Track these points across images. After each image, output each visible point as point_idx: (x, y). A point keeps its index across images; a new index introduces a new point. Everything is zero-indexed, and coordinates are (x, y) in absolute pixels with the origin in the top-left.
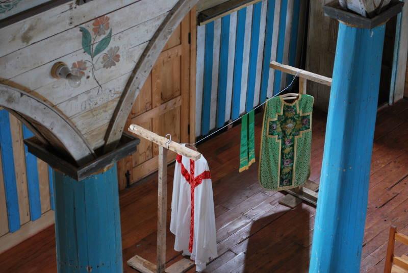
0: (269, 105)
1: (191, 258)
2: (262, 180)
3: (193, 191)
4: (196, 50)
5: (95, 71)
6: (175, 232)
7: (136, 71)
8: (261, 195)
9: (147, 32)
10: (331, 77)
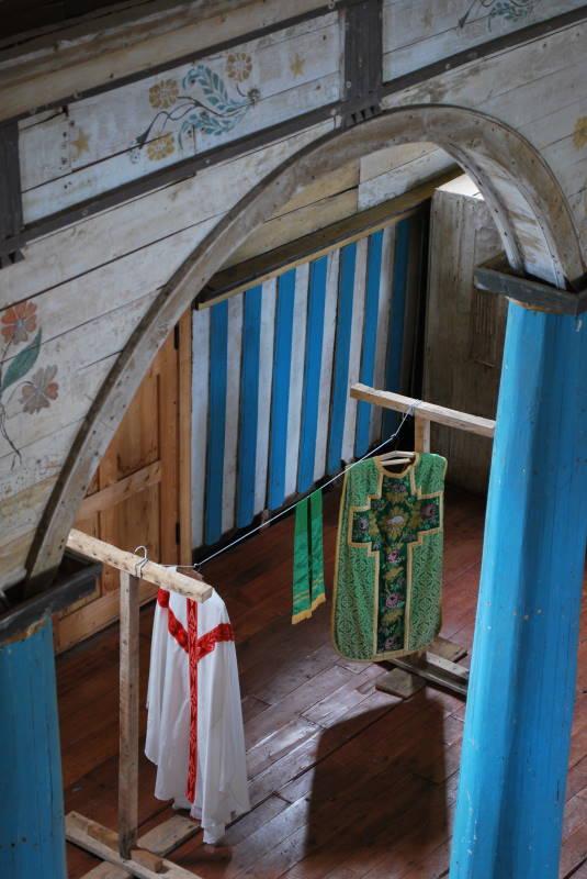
0: (353, 477)
1: (192, 814)
2: (340, 638)
3: (194, 667)
4: (192, 363)
5: (7, 421)
6: (156, 758)
7: (94, 419)
8: (338, 673)
9: (116, 334)
10: (490, 413)
